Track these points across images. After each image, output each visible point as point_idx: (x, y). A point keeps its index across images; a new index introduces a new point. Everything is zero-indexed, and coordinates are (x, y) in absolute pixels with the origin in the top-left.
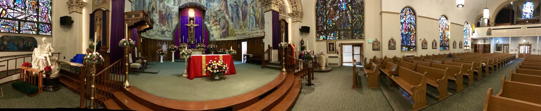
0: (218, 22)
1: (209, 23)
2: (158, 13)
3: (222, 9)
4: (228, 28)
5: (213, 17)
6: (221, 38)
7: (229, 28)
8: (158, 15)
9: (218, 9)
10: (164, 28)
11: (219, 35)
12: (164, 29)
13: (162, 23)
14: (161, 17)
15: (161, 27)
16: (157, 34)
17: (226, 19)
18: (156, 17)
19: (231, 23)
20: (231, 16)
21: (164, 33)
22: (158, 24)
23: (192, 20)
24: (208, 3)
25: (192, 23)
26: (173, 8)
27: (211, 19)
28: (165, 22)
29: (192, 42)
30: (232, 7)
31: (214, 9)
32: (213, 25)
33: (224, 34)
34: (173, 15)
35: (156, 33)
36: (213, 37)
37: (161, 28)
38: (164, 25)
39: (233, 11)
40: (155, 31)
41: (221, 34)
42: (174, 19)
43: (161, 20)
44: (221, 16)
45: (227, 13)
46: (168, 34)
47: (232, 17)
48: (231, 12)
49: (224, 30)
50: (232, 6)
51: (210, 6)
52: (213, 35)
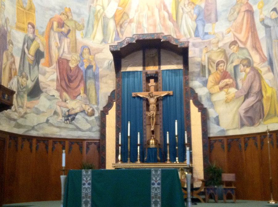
0: (230, 77)
1: (205, 83)
2: (55, 65)
3: (242, 36)
4: (260, 93)
5: (214, 66)
6: (242, 125)
7: (264, 93)
8: (55, 71)
9: (229, 38)
10: (74, 105)
11: (237, 118)
12: (73, 109)
13: (67, 92)
14: (65, 75)
15: (65, 101)
16: (51, 121)
17: (255, 65)
18: (47, 75)
19: (267, 77)
20: (266, 54)
21: (73, 119)
22: (57, 94)
23: (152, 81)
24: (200, 28)
25: (152, 89)
26: (99, 51)
27: (210, 72)
28: (76, 90)
29: (152, 142)
30: (267, 27)
31: (218, 42)
32: (217, 88)
33: (249, 114)
34: (100, 70)
35: (47, 121)
36: (218, 124)
37: (63, 104)
38: (74, 98)
39: (270, 36)
40: (43, 112)
41: (242, 112)
42: (104, 80)
43: (64, 84)
44: (238, 58)
45: (256, 47)
46: (87, 120)
47: (269, 55)
48: (267, 43)
49: (251, 100)
50: (267, 22)
51: (206, 34)
52: (218, 122)
